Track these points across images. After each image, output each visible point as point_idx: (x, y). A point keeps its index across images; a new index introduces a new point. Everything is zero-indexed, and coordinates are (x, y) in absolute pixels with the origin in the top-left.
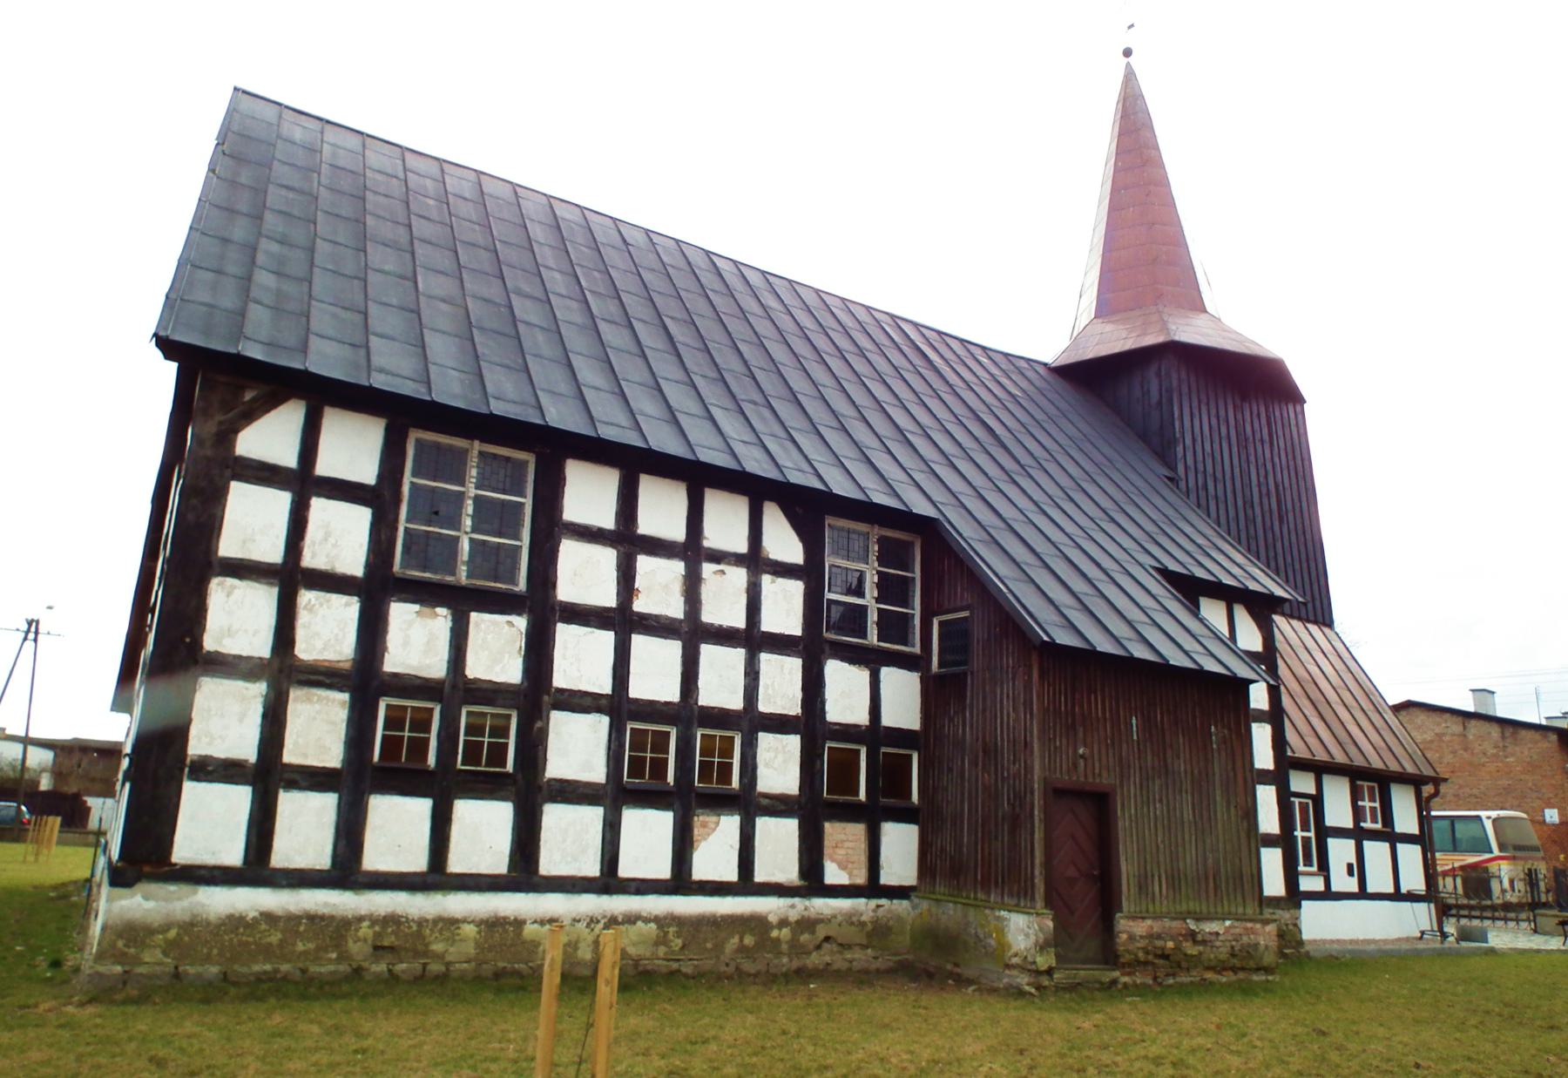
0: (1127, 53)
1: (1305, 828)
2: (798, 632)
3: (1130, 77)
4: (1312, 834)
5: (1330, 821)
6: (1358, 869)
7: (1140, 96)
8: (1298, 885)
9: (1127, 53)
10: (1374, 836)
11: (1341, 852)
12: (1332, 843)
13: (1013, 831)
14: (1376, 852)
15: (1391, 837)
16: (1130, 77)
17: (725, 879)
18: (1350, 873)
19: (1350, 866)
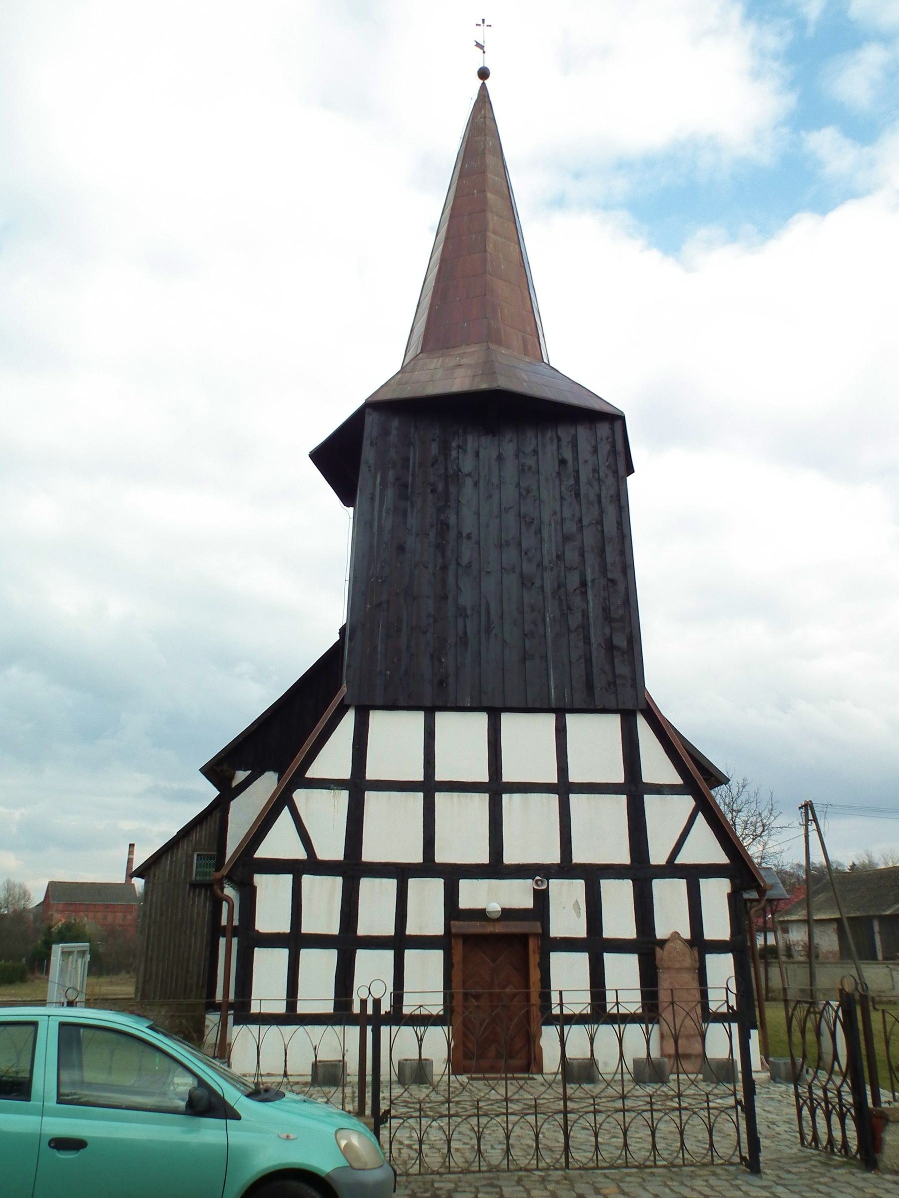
0: (484, 74)
3: (483, 101)
9: (484, 74)
16: (483, 101)
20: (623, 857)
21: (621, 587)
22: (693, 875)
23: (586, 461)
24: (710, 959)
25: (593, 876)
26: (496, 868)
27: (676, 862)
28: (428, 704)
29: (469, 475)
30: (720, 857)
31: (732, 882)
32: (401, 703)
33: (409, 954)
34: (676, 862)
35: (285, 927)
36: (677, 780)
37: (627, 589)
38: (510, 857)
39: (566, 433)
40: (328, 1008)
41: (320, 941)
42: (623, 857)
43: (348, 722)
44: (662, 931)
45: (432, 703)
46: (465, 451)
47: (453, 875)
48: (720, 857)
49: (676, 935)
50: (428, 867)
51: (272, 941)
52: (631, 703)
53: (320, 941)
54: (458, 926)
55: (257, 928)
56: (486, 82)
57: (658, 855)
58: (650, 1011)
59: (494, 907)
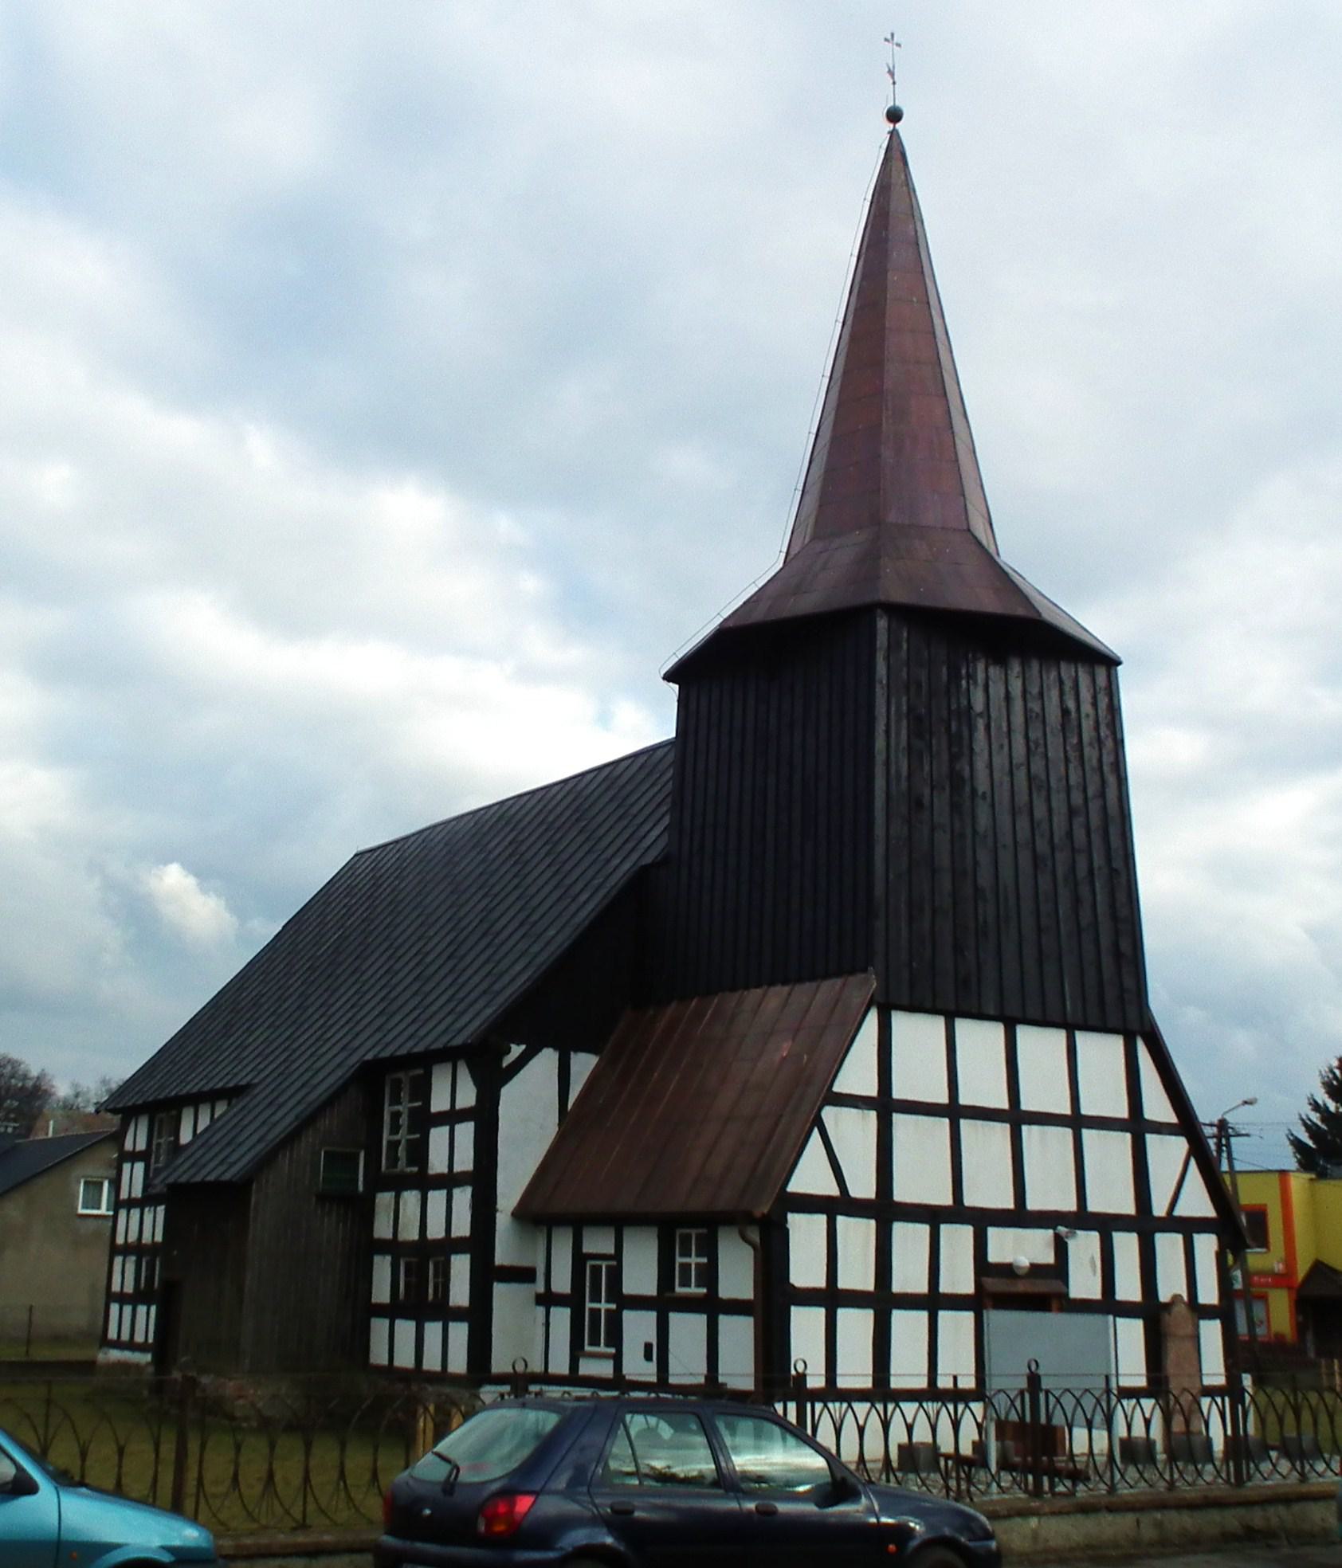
0: (894, 116)
1: (595, 1313)
2: (895, 1115)
3: (895, 155)
4: (589, 1305)
5: (629, 1287)
6: (659, 1351)
7: (916, 244)
8: (457, 1252)
9: (894, 116)
10: (689, 1305)
11: (639, 1327)
12: (628, 1316)
13: (954, 758)
14: (688, 1329)
15: (713, 1307)
16: (895, 155)
17: (1094, 1132)
18: (648, 1356)
19: (648, 1347)
20: (1129, 1208)
21: (1123, 880)
22: (1188, 1227)
23: (1087, 716)
24: (628, 1316)
25: (1106, 1225)
26: (1019, 1217)
27: (791, 1188)
28: (952, 1007)
29: (980, 715)
30: (1208, 1211)
31: (406, 1189)
32: (928, 1005)
33: (943, 1315)
34: (791, 1188)
35: (923, 1288)
36: (1173, 1119)
37: (1129, 881)
38: (1032, 1204)
39: (1067, 670)
40: (867, 1383)
41: (910, 1302)
42: (1129, 1208)
43: (872, 1020)
44: (1164, 1296)
45: (953, 1008)
46: (976, 683)
47: (982, 1220)
48: (1208, 1211)
49: (1176, 1298)
50: (957, 1212)
51: (809, 1297)
52: (1136, 1025)
53: (910, 1302)
54: (993, 1284)
55: (792, 1280)
56: (898, 126)
57: (1159, 1209)
58: (1157, 1385)
59: (1024, 1261)
